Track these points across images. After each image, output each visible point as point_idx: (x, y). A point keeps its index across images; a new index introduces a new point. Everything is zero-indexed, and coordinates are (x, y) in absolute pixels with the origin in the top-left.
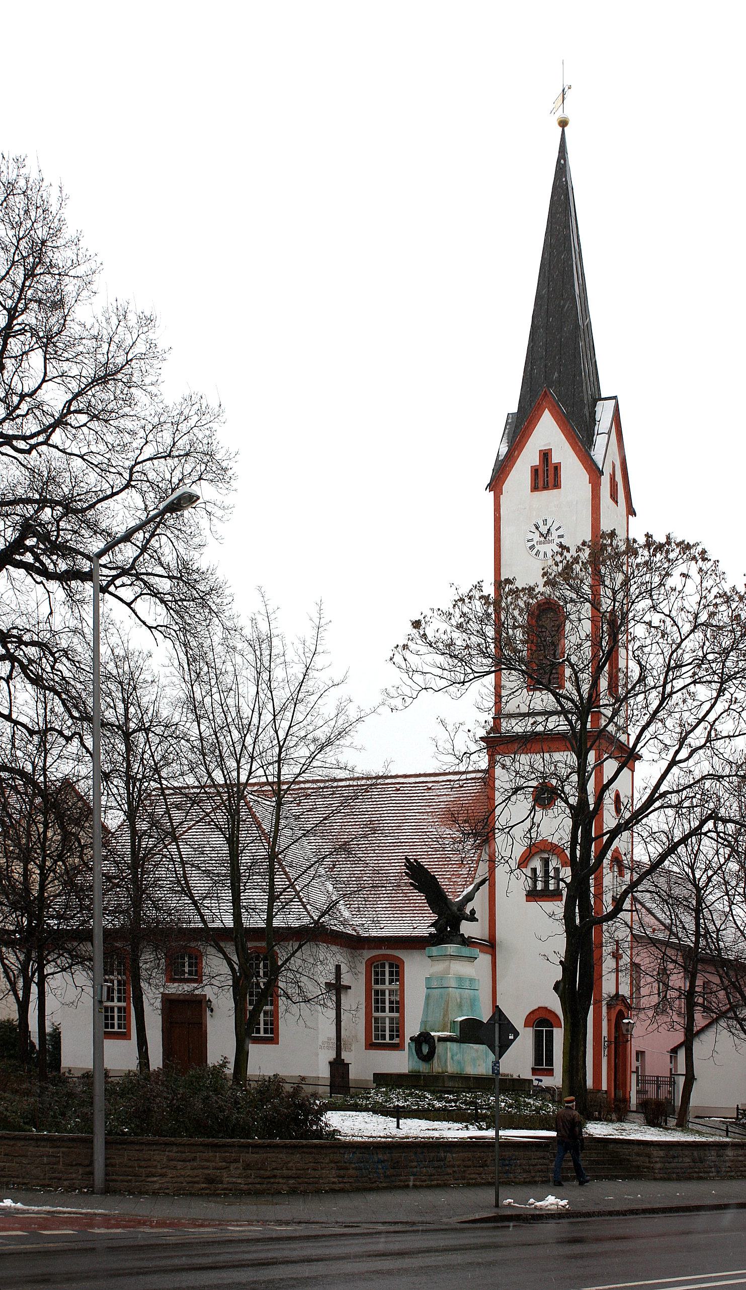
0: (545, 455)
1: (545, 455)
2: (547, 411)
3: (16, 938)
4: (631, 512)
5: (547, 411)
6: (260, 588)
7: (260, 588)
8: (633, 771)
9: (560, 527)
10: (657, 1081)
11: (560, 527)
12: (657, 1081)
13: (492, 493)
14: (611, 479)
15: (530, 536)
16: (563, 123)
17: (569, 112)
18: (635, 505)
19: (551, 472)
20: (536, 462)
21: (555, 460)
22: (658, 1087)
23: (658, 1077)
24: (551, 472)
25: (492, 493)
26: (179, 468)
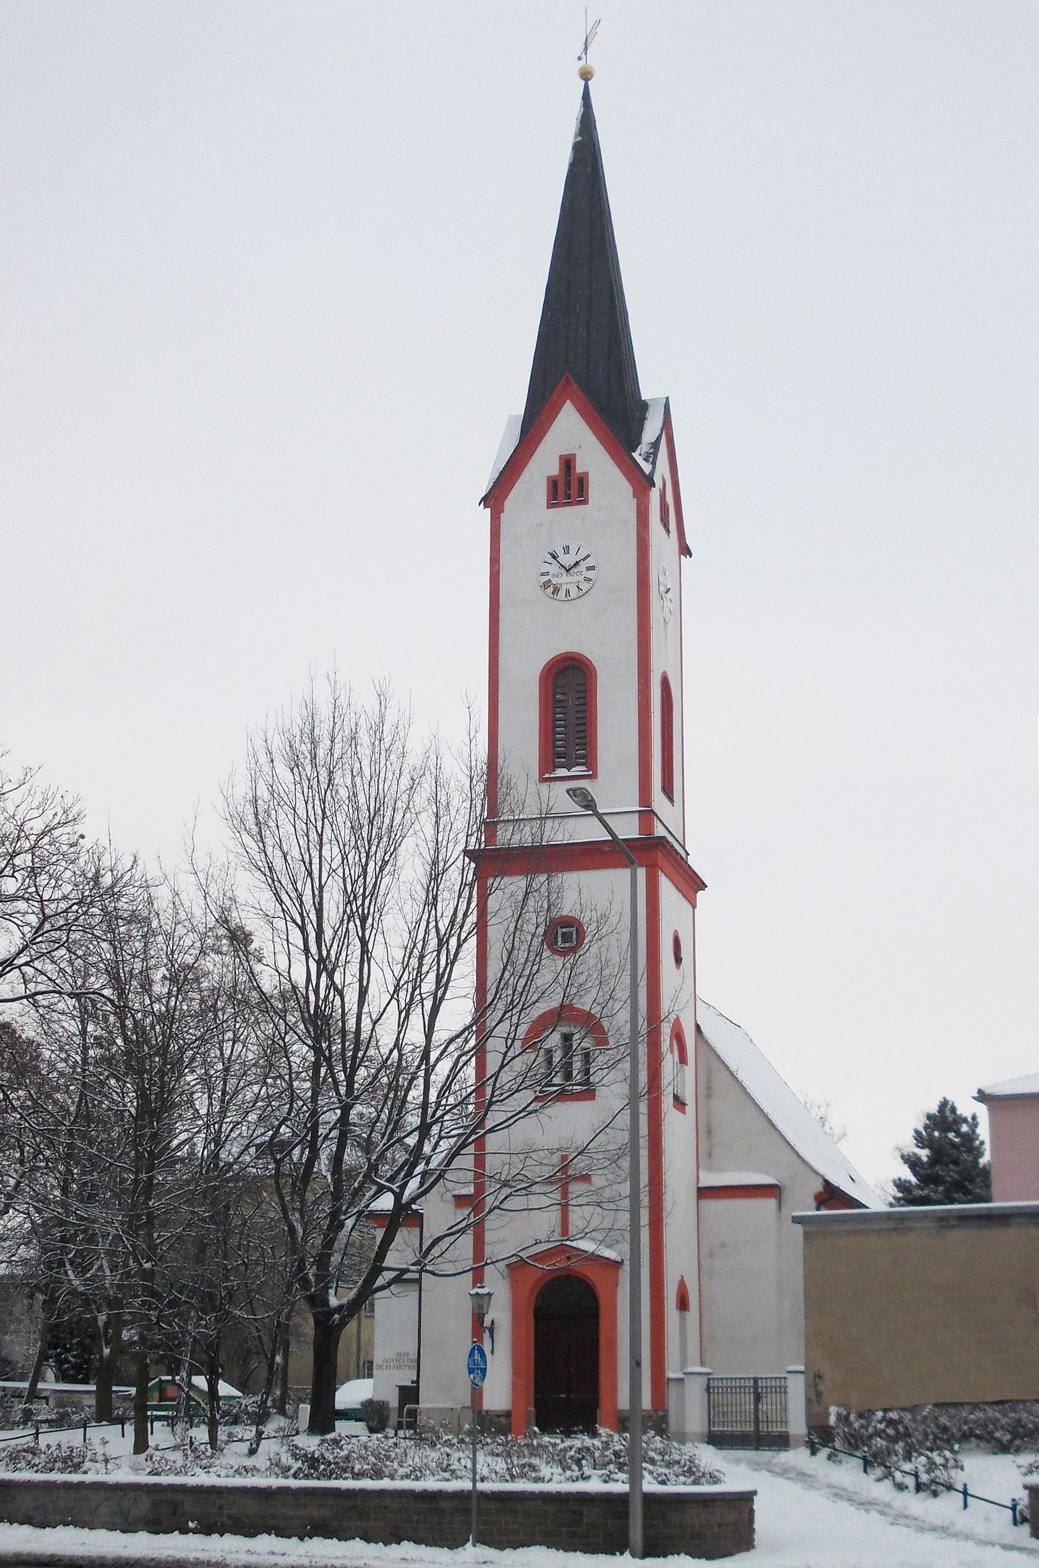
0: (568, 463)
1: (568, 463)
2: (568, 402)
3: (559, 1428)
4: (685, 550)
5: (568, 402)
6: (123, 1436)
7: (123, 1436)
8: (694, 907)
9: (588, 556)
10: (756, 1387)
11: (588, 556)
12: (756, 1387)
13: (489, 510)
14: (661, 498)
15: (546, 568)
16: (586, 76)
17: (593, 61)
18: (689, 541)
19: (574, 484)
20: (554, 470)
21: (579, 469)
22: (758, 1398)
23: (756, 1380)
24: (574, 484)
25: (489, 510)
26: (69, 852)
